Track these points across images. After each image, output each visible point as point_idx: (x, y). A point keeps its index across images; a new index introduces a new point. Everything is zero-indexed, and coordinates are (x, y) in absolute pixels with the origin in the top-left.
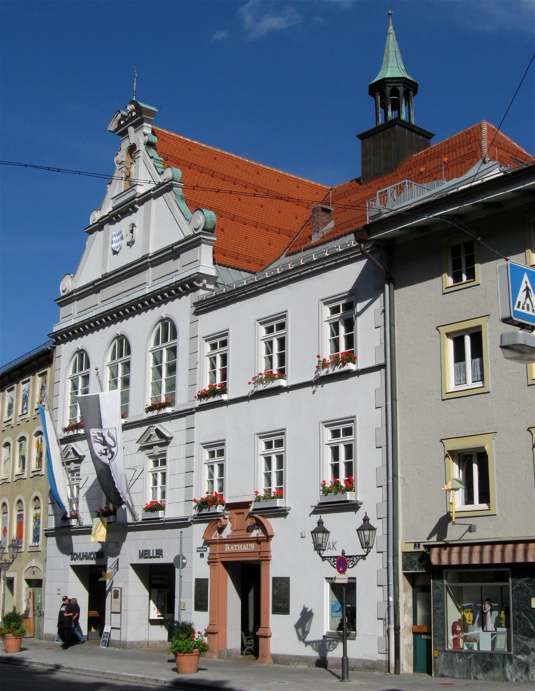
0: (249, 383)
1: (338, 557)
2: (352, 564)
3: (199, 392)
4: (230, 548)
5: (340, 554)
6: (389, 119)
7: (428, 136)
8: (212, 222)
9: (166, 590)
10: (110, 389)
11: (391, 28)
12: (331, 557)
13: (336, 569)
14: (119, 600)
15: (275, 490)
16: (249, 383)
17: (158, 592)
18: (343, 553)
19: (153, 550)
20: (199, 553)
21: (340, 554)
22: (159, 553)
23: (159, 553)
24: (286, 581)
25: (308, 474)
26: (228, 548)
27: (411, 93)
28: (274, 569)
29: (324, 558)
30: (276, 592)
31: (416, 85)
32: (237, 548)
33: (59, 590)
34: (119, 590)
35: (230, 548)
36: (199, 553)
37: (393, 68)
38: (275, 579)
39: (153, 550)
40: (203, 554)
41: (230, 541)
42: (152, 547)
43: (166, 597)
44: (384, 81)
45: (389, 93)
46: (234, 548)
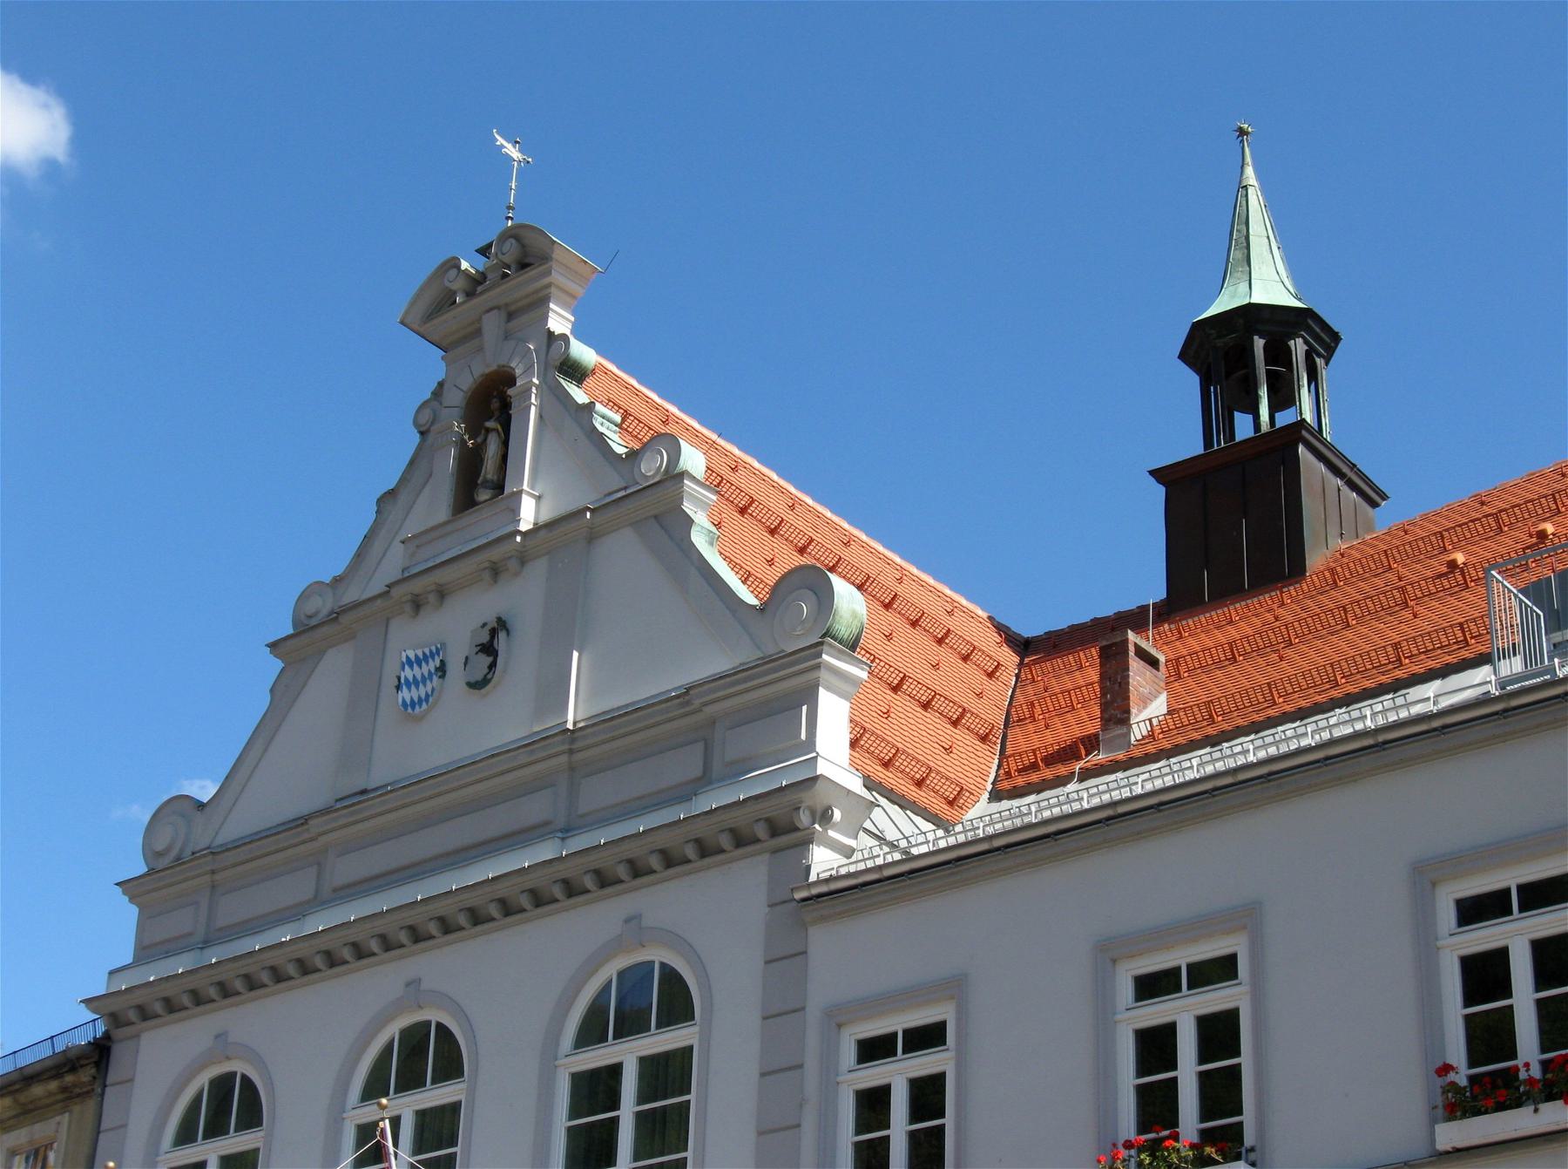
8: (854, 615)
37: (1270, 284)
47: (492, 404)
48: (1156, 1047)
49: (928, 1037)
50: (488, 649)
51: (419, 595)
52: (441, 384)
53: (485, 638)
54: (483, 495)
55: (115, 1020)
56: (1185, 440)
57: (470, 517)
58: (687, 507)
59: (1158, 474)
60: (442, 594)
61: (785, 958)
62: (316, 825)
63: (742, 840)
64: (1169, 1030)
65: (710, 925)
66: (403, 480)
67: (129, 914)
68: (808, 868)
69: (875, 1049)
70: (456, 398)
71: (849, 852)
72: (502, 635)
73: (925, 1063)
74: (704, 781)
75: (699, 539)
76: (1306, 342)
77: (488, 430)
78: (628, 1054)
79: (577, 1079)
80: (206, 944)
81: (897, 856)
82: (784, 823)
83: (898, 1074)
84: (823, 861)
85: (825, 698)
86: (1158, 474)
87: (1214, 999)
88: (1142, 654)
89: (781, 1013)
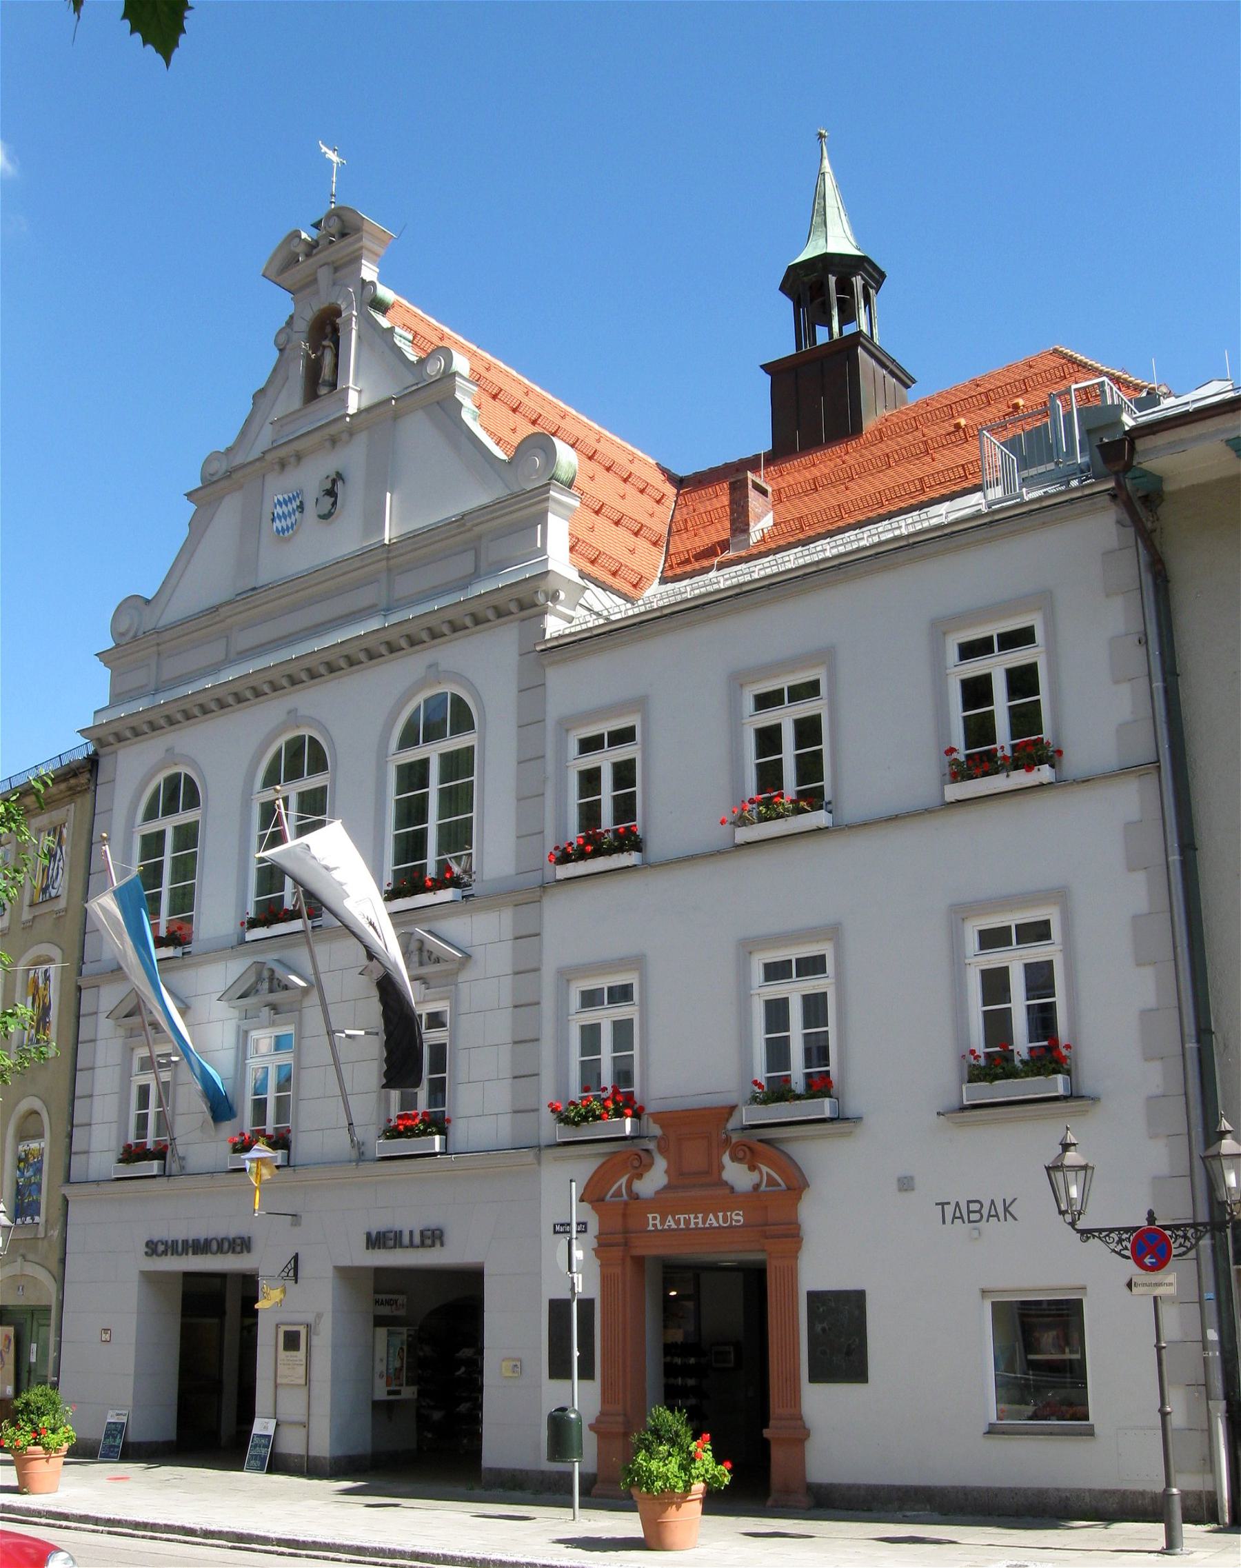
0: (723, 822)
1: (1135, 1229)
2: (1181, 1245)
3: (557, 848)
4: (663, 1222)
5: (1142, 1222)
6: (819, 343)
7: (906, 380)
8: (570, 465)
9: (404, 1330)
10: (819, 716)
11: (826, 163)
12: (1111, 1230)
13: (1131, 1262)
14: (301, 1354)
15: (1025, 1056)
16: (723, 822)
17: (390, 1334)
18: (1151, 1217)
19: (411, 1232)
21: (1142, 1222)
22: (433, 1237)
24: (857, 1300)
25: (903, 1032)
27: (872, 292)
28: (819, 1269)
29: (1086, 1234)
30: (819, 1328)
31: (883, 275)
32: (687, 1222)
34: (303, 1331)
35: (663, 1223)
37: (839, 239)
38: (812, 1296)
39: (411, 1232)
42: (409, 1221)
43: (405, 1347)
44: (827, 262)
45: (820, 287)
46: (678, 1222)
47: (326, 329)
48: (768, 739)
49: (623, 736)
50: (331, 493)
51: (284, 458)
52: (292, 317)
53: (329, 486)
54: (323, 391)
55: (100, 742)
56: (785, 347)
57: (316, 406)
58: (458, 395)
59: (765, 367)
60: (299, 457)
61: (531, 689)
62: (224, 611)
63: (500, 613)
64: (986, 680)
65: (483, 669)
66: (270, 382)
67: (103, 675)
68: (544, 630)
69: (590, 745)
70: (302, 326)
71: (570, 620)
72: (339, 483)
73: (622, 753)
74: (477, 575)
75: (466, 416)
76: (863, 278)
77: (324, 347)
78: (432, 752)
79: (401, 769)
80: (157, 691)
81: (601, 621)
82: (528, 602)
83: (605, 760)
84: (554, 626)
85: (552, 519)
86: (765, 367)
87: (805, 709)
88: (757, 487)
89: (530, 722)
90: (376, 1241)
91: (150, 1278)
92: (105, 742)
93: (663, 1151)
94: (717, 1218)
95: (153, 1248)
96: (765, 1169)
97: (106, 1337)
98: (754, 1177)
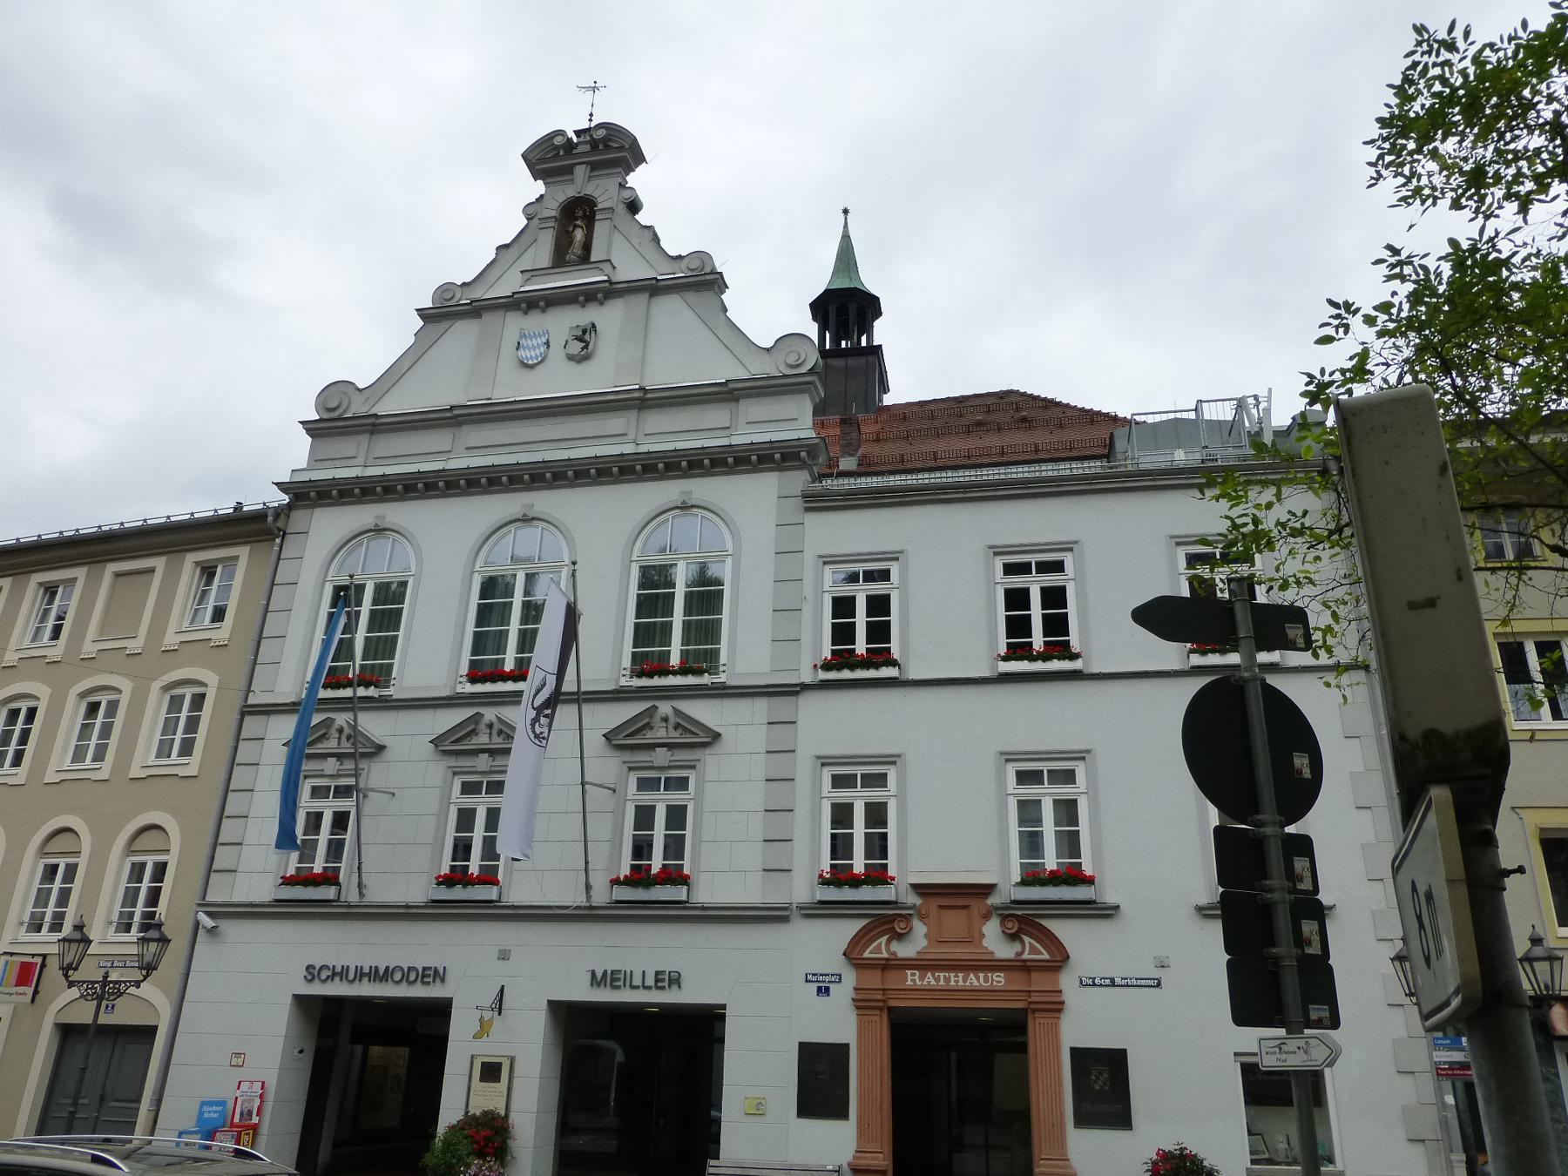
20: (815, 986)
23: (675, 980)
26: (912, 978)
32: (947, 980)
33: (238, 1055)
36: (815, 986)
40: (827, 990)
41: (923, 965)
46: (937, 980)
90: (596, 981)
91: (301, 1001)
92: (305, 495)
93: (922, 917)
94: (978, 979)
95: (312, 973)
96: (1027, 939)
97: (240, 1061)
98: (1017, 947)
